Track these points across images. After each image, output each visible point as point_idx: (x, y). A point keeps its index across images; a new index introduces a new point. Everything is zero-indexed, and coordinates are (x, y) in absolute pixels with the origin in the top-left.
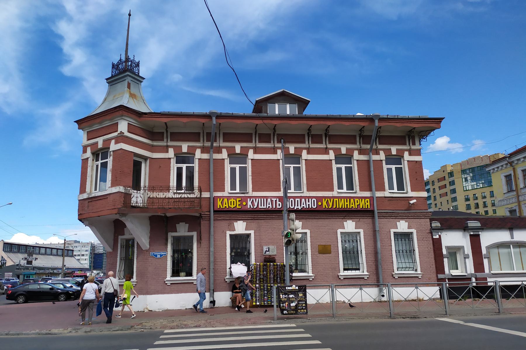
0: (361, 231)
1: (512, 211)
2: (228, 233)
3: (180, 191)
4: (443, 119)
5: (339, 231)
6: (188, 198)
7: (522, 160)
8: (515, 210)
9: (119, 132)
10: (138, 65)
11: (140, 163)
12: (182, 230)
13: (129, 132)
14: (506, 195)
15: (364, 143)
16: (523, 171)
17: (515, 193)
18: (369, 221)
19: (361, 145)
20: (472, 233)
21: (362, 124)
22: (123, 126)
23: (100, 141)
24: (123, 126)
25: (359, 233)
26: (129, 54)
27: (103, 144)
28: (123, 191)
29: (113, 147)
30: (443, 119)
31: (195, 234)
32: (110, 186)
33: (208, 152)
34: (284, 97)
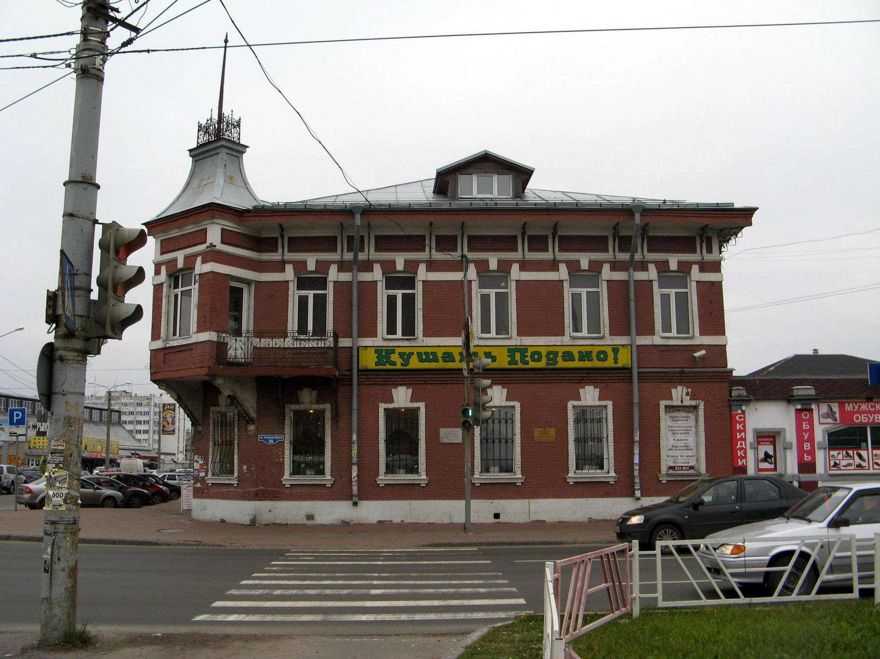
0: (609, 404)
2: (382, 406)
3: (302, 337)
4: (756, 209)
5: (570, 404)
9: (208, 244)
10: (238, 124)
11: (241, 290)
12: (308, 401)
13: (223, 242)
15: (621, 250)
19: (617, 253)
20: (799, 407)
22: (214, 235)
23: (180, 256)
24: (214, 235)
25: (606, 407)
26: (224, 110)
27: (185, 261)
28: (215, 339)
29: (200, 268)
30: (756, 209)
31: (327, 407)
32: (195, 330)
33: (350, 270)
34: (486, 163)
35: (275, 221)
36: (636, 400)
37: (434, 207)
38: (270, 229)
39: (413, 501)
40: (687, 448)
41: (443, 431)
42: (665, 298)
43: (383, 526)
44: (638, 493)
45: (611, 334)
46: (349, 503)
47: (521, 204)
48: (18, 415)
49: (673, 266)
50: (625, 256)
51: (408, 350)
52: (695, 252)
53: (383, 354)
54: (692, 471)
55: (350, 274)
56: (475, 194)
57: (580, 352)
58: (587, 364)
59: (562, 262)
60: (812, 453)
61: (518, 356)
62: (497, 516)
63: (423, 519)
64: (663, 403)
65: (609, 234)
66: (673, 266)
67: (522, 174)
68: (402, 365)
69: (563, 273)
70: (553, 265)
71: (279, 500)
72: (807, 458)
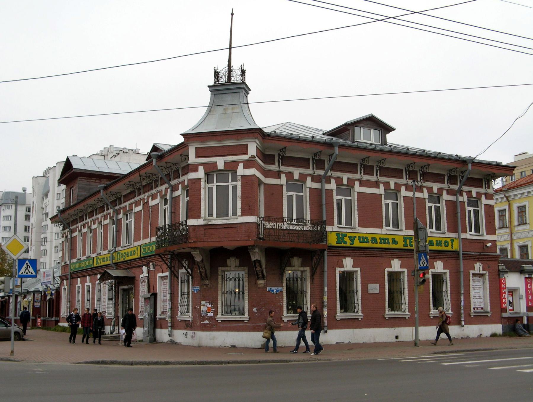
0: (448, 271)
5: (387, 270)
7: (520, 196)
8: (506, 249)
16: (518, 207)
17: (508, 230)
18: (453, 261)
20: (527, 276)
22: (253, 149)
31: (308, 269)
32: (240, 214)
34: (372, 122)
35: (282, 145)
36: (462, 270)
37: (373, 147)
38: (280, 149)
39: (229, 332)
40: (480, 297)
41: (370, 286)
42: (290, 198)
44: (463, 323)
45: (406, 229)
49: (296, 177)
50: (321, 173)
51: (353, 235)
52: (482, 187)
53: (341, 236)
54: (482, 311)
56: (362, 140)
57: (437, 241)
58: (439, 248)
61: (408, 241)
62: (397, 337)
64: (471, 272)
66: (296, 177)
67: (386, 129)
69: (283, 180)
70: (376, 185)
71: (280, 331)
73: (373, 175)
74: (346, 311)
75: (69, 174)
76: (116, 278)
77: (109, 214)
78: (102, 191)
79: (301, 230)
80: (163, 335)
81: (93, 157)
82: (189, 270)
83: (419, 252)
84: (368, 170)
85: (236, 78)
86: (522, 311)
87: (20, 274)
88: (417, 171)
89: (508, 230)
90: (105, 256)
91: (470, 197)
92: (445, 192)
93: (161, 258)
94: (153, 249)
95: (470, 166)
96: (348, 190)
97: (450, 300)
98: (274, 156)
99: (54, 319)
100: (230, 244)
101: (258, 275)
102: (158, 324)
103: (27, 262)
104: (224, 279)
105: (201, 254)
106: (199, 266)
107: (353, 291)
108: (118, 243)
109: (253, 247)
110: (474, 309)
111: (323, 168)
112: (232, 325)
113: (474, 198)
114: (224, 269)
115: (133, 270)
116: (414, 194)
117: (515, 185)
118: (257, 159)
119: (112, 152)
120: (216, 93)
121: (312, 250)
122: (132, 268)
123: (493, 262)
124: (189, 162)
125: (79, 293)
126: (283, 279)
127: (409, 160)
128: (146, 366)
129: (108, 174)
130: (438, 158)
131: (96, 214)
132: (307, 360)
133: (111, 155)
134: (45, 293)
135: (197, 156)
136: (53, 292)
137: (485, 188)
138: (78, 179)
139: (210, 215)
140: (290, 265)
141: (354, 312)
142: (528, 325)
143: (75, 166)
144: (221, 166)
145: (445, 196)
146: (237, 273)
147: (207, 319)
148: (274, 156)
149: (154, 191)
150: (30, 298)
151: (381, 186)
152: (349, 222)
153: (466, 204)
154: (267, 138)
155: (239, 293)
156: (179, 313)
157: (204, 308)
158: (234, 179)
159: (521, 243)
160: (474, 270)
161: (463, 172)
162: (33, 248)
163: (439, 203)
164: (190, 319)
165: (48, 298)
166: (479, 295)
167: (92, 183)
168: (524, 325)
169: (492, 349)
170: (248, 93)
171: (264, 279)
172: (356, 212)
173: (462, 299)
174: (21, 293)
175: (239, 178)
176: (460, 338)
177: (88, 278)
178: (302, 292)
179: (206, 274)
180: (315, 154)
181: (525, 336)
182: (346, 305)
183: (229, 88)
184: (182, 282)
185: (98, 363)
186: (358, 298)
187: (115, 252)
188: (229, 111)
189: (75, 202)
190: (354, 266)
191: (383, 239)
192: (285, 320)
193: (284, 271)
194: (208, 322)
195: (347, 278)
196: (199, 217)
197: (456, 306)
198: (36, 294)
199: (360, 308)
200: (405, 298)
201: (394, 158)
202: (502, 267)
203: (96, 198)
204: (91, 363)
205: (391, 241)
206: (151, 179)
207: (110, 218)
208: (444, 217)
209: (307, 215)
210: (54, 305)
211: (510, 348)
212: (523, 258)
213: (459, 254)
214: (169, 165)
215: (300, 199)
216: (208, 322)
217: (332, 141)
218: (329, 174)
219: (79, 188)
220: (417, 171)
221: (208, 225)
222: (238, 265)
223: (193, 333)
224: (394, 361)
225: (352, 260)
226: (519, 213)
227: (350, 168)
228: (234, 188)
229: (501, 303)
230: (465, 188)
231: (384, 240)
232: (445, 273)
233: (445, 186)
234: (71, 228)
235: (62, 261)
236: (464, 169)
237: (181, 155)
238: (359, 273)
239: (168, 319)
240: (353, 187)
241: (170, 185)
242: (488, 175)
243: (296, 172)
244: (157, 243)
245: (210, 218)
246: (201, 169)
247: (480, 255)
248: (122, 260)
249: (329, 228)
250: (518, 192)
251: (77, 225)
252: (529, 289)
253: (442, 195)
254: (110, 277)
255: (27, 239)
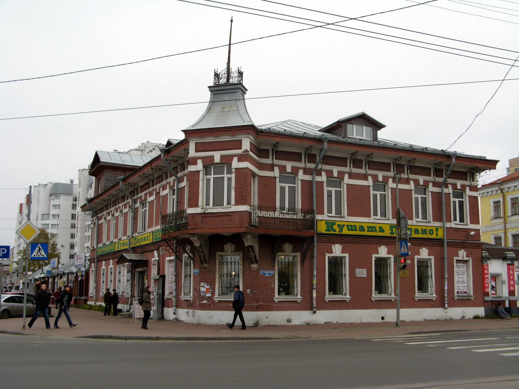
0: (433, 258)
1: (498, 239)
4: (499, 161)
6: (291, 219)
7: (513, 188)
8: (500, 238)
14: (492, 222)
16: (512, 199)
17: (502, 220)
18: (438, 249)
20: (509, 263)
21: (439, 160)
22: (246, 145)
24: (246, 145)
30: (499, 161)
31: (298, 254)
34: (363, 119)
35: (274, 140)
36: (446, 256)
38: (273, 144)
41: (358, 271)
42: (283, 189)
43: (328, 325)
44: (446, 306)
46: (310, 312)
47: (376, 143)
48: (3, 251)
49: (289, 170)
50: (312, 166)
51: (342, 223)
52: (467, 180)
53: (330, 224)
54: (466, 294)
55: (440, 189)
56: (355, 136)
57: (422, 230)
58: (424, 236)
59: (411, 180)
60: (513, 286)
62: (383, 318)
63: (208, 321)
64: (455, 258)
65: (270, 149)
66: (289, 170)
67: (377, 126)
68: (339, 232)
69: (276, 173)
70: (365, 177)
71: (272, 310)
72: (512, 288)
73: (362, 168)
74: (335, 293)
75: (98, 168)
76: (130, 261)
77: (129, 203)
78: (121, 182)
79: (264, 217)
80: (169, 313)
81: (132, 152)
82: (191, 254)
83: (401, 240)
84: (357, 163)
85: (234, 80)
86: (504, 295)
87: (33, 256)
88: (404, 165)
89: (502, 220)
90: (125, 241)
91: (455, 189)
92: (431, 185)
93: (167, 243)
94: (159, 236)
95: (454, 160)
96: (337, 182)
97: (434, 284)
98: (268, 150)
99: (83, 298)
100: (226, 231)
101: (251, 260)
102: (166, 302)
103: (39, 245)
104: (221, 263)
105: (199, 239)
106: (198, 251)
107: (342, 276)
108: (134, 230)
109: (246, 233)
110: (458, 292)
111: (314, 162)
112: (228, 305)
113: (459, 190)
114: (221, 253)
115: (147, 254)
116: (397, 186)
117: (509, 178)
118: (251, 153)
119: (149, 148)
120: (215, 93)
121: (302, 237)
122: (146, 252)
123: (477, 250)
124: (189, 156)
125: (103, 274)
126: (274, 263)
127: (396, 155)
128: (138, 341)
129: (132, 167)
130: (424, 153)
131: (119, 203)
132: (287, 338)
133: (148, 150)
134: (77, 275)
135: (197, 151)
136: (83, 274)
137: (470, 180)
138: (105, 171)
139: (208, 204)
140: (282, 251)
141: (342, 294)
142: (509, 308)
143: (102, 160)
144: (217, 159)
145: (431, 188)
146: (233, 257)
147: (205, 299)
148: (268, 151)
149: (164, 183)
150: (65, 279)
151: (370, 178)
152: (339, 211)
153: (451, 195)
154: (261, 134)
155: (235, 275)
156: (183, 294)
157: (203, 289)
158: (229, 172)
159: (514, 232)
160: (458, 256)
161: (448, 166)
162: (79, 234)
163: (425, 195)
164: (191, 299)
165: (79, 279)
166: (463, 280)
167: (117, 175)
168: (506, 309)
169: (467, 331)
170: (245, 93)
171: (257, 263)
172: (346, 202)
173: (446, 283)
174: (58, 275)
175: (233, 170)
176: (444, 319)
177: (111, 261)
178: (292, 276)
179: (204, 258)
180: (307, 149)
181: (506, 319)
182: (335, 288)
183: (227, 88)
184: (185, 265)
185: (96, 337)
186: (346, 282)
187: (132, 237)
188: (227, 109)
189: (103, 191)
190: (342, 252)
191: (370, 227)
192: (276, 301)
193: (275, 256)
194: (206, 302)
195: (336, 264)
196: (197, 206)
197: (440, 290)
198: (70, 276)
199: (348, 291)
200: (391, 282)
201: (382, 153)
202: (485, 254)
203: (117, 188)
204: (90, 337)
205: (378, 229)
206: (162, 171)
207: (130, 207)
208: (429, 208)
209: (299, 205)
210: (82, 284)
211: (485, 330)
212: (516, 246)
213: (443, 242)
214: (175, 159)
215: (292, 191)
216: (206, 302)
217: (324, 137)
218: (319, 167)
219: (106, 179)
220: (404, 165)
221: (205, 213)
222: (234, 250)
223: (193, 312)
224: (368, 341)
225: (341, 246)
226: (512, 204)
227: (341, 161)
228: (229, 179)
229: (484, 287)
230: (450, 181)
231: (371, 228)
232: (430, 259)
233: (431, 178)
234: (98, 216)
235: (91, 246)
236: (448, 163)
237: (184, 150)
238: (347, 259)
239: (174, 299)
240: (343, 179)
241: (177, 177)
242: (473, 169)
243: (289, 166)
244: (164, 230)
245: (208, 207)
246: (200, 162)
247: (464, 242)
248: (138, 245)
249: (318, 217)
250: (512, 185)
251: (103, 213)
252: (511, 275)
253: (428, 187)
254: (126, 260)
255: (73, 226)
